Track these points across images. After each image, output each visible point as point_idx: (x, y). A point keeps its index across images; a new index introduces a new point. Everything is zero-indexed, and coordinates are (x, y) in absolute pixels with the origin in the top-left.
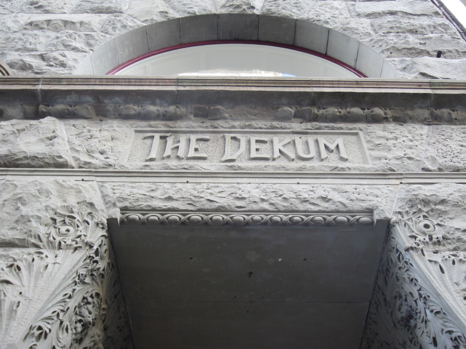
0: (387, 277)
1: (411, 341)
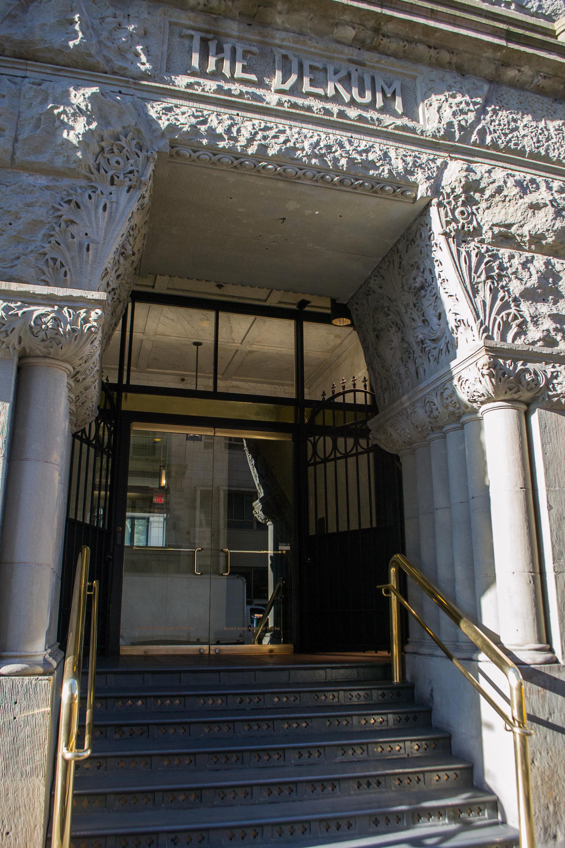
0: (410, 246)
1: (415, 306)
